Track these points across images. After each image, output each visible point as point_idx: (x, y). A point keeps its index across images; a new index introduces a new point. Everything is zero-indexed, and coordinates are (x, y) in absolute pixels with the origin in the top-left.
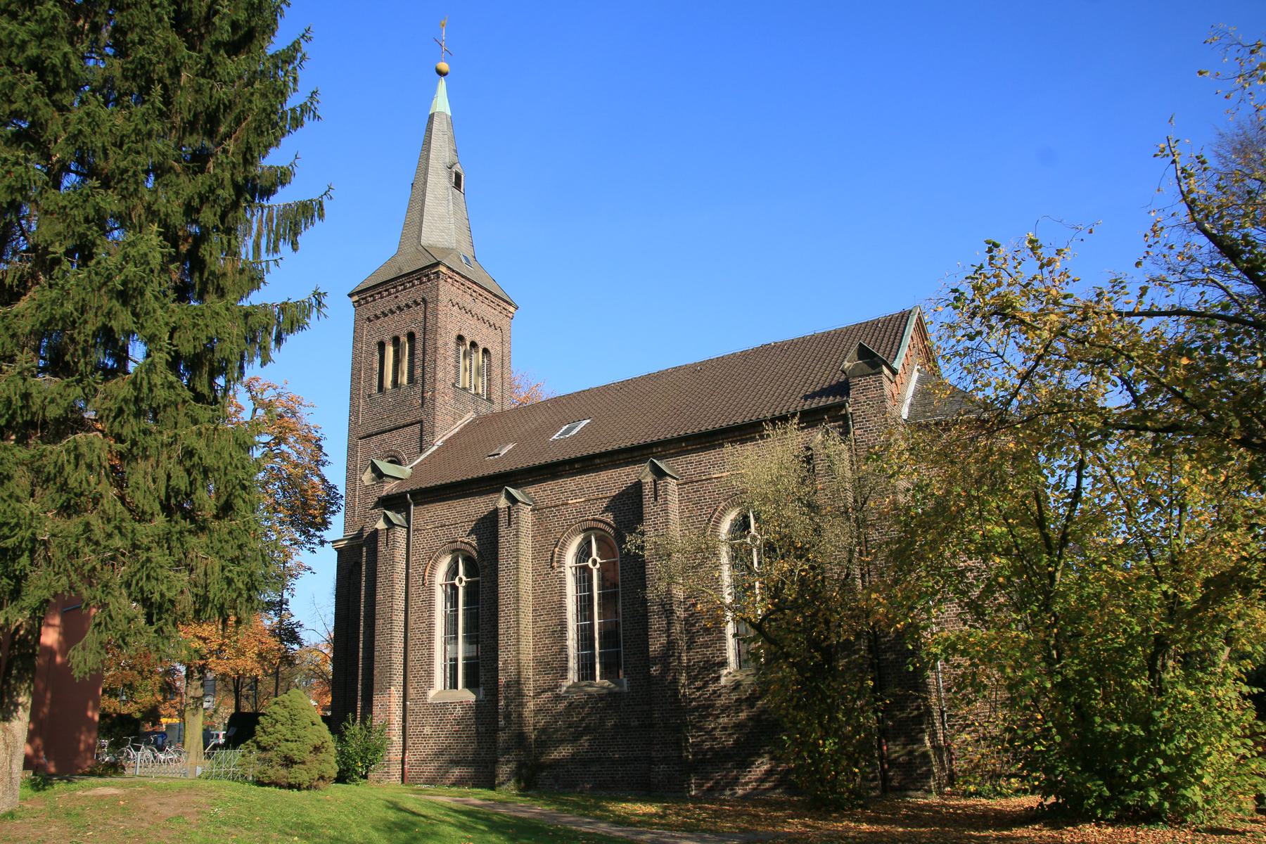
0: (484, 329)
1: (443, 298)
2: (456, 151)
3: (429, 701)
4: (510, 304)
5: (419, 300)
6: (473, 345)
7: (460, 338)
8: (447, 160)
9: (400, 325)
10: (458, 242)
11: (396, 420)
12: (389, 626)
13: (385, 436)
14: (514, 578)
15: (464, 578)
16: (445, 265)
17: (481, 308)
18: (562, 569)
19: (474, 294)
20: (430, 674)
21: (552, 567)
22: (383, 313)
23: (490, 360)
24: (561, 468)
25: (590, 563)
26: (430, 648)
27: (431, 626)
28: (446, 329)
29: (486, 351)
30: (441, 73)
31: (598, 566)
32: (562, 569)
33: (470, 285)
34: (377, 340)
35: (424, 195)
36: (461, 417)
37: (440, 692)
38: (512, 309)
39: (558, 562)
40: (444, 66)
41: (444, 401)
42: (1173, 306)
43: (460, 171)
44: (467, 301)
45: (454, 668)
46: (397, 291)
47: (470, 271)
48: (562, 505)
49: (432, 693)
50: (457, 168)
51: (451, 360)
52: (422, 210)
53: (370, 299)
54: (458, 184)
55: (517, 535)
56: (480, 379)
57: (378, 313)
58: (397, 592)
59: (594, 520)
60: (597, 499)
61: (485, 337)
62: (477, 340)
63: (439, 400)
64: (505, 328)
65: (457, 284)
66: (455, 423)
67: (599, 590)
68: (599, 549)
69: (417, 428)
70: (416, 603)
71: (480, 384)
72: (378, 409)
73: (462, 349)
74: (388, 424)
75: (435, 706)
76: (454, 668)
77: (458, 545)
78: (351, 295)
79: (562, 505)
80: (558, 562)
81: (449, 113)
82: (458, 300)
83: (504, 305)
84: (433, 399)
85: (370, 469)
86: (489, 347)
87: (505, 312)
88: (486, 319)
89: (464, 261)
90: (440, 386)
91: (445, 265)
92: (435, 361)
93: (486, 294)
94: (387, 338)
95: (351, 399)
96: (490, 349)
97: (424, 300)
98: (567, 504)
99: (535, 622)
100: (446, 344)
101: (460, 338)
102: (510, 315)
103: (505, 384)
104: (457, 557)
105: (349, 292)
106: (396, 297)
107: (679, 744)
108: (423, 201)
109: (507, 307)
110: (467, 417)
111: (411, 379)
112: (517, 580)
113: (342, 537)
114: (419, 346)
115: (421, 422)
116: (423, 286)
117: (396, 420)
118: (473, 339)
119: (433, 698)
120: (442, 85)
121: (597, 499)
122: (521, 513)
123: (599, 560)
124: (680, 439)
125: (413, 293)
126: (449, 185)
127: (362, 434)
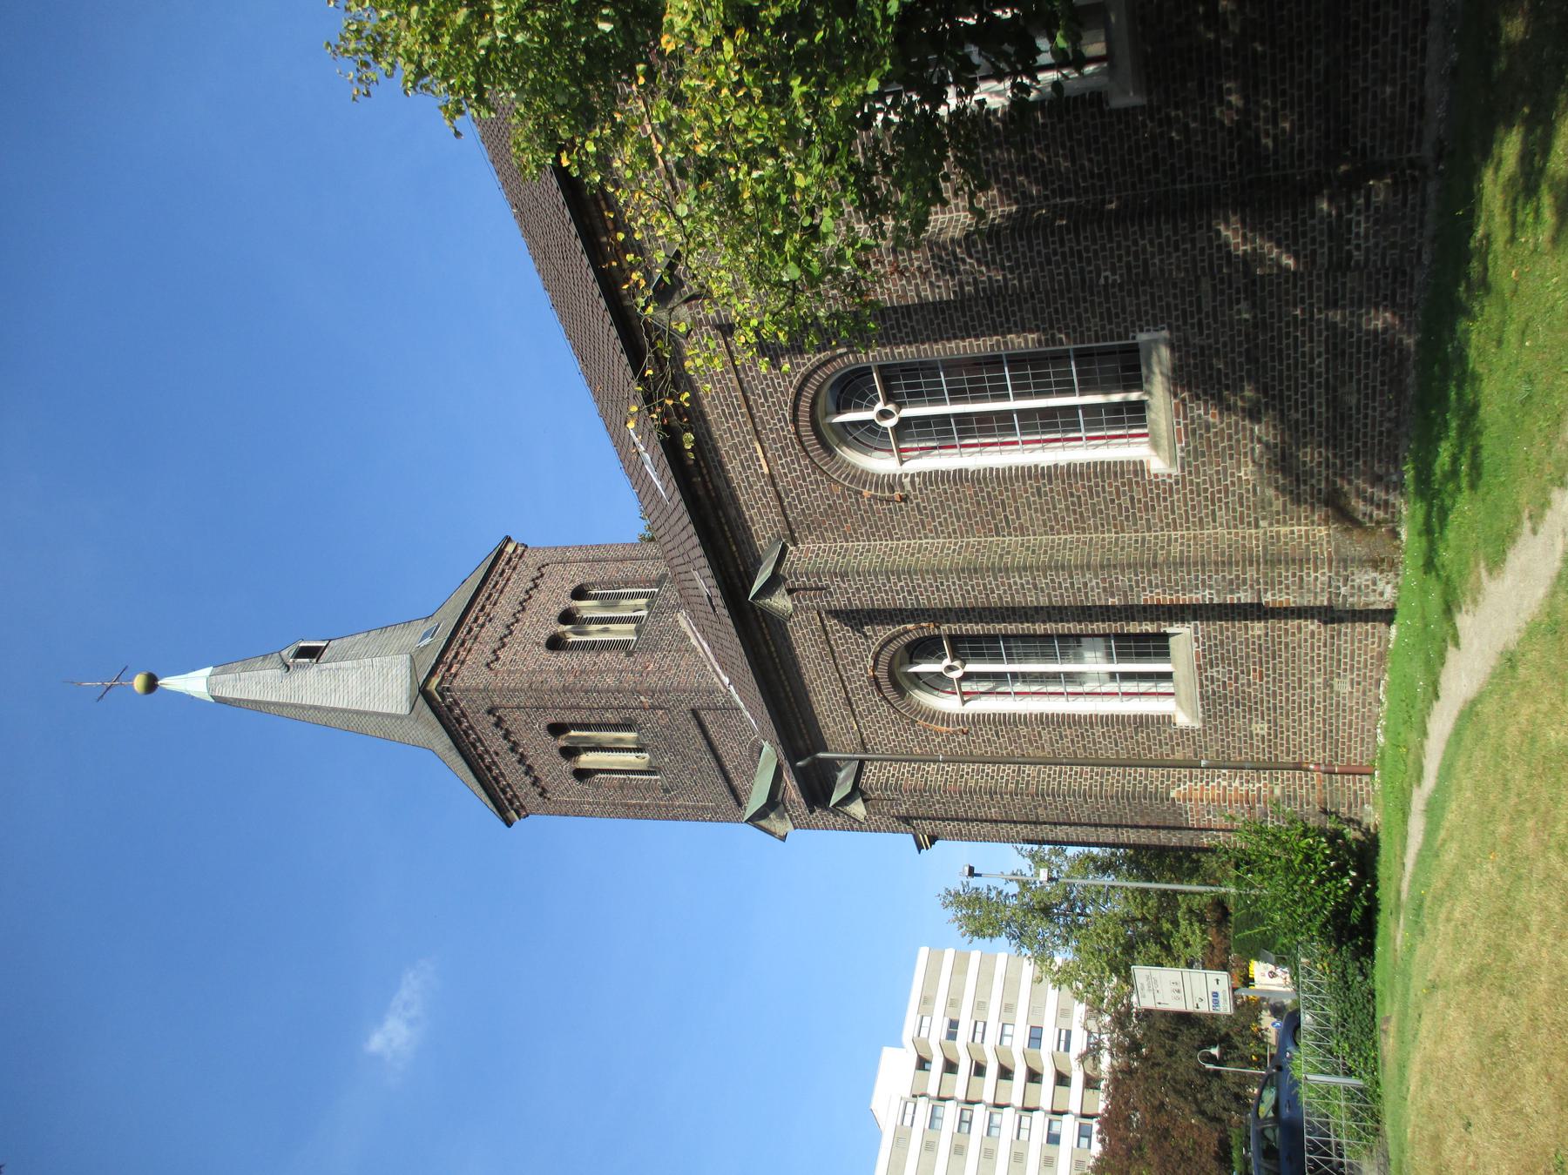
0: (540, 597)
1: (484, 678)
2: (265, 656)
3: (1198, 725)
4: (501, 552)
5: (493, 719)
6: (567, 617)
7: (555, 643)
8: (278, 672)
9: (542, 752)
10: (399, 652)
11: (698, 750)
12: (1049, 799)
13: (729, 766)
14: (929, 578)
15: (947, 662)
16: (427, 680)
17: (504, 608)
18: (906, 481)
19: (481, 621)
20: (1141, 722)
21: (904, 499)
22: (526, 773)
23: (593, 585)
24: (701, 492)
25: (889, 423)
26: (1091, 721)
27: (1044, 720)
28: (534, 671)
29: (579, 593)
30: (152, 684)
31: (891, 407)
32: (906, 481)
33: (464, 629)
34: (572, 780)
35: (334, 710)
36: (685, 638)
37: (1179, 703)
38: (510, 548)
39: (892, 489)
40: (139, 682)
41: (657, 670)
42: (1519, 631)
43: (293, 649)
44: (492, 632)
45: (1127, 676)
46: (487, 752)
47: (443, 629)
48: (774, 485)
49: (1183, 720)
50: (288, 653)
51: (588, 658)
52: (357, 712)
53: (510, 793)
54: (311, 653)
55: (844, 575)
56: (624, 602)
57: (528, 780)
58: (982, 783)
59: (795, 421)
60: (752, 417)
61: (556, 597)
62: (557, 610)
63: (652, 681)
64: (540, 558)
65: (463, 654)
66: (694, 649)
67: (942, 402)
68: (858, 407)
69: (708, 718)
70: (1003, 746)
71: (632, 602)
72: (686, 776)
73: (573, 638)
74: (708, 760)
75: (1208, 716)
76: (1127, 676)
77: (882, 674)
78: (509, 823)
79: (774, 485)
80: (892, 489)
81: (208, 671)
82: (488, 650)
83: (501, 565)
84: (651, 692)
85: (763, 823)
86: (570, 587)
87: (515, 560)
88: (524, 596)
89: (428, 640)
90: (630, 680)
91: (427, 680)
92: (586, 692)
93: (481, 599)
94: (567, 766)
95: (676, 818)
96: (573, 586)
97: (490, 712)
98: (771, 476)
99: (1022, 530)
100: (559, 671)
101: (555, 643)
102: (519, 551)
103: (634, 554)
104: (908, 675)
105: (503, 825)
106: (497, 754)
107: (1394, 178)
108: (344, 711)
109: (505, 557)
110: (683, 624)
111: (627, 726)
112: (936, 572)
113: (911, 836)
114: (569, 717)
115: (695, 713)
116: (469, 712)
117: (698, 750)
118: (554, 618)
119: (1194, 716)
120: (170, 683)
121: (752, 417)
122: (799, 566)
123: (880, 406)
124: (594, 252)
125: (484, 726)
126: (315, 668)
127: (732, 802)
